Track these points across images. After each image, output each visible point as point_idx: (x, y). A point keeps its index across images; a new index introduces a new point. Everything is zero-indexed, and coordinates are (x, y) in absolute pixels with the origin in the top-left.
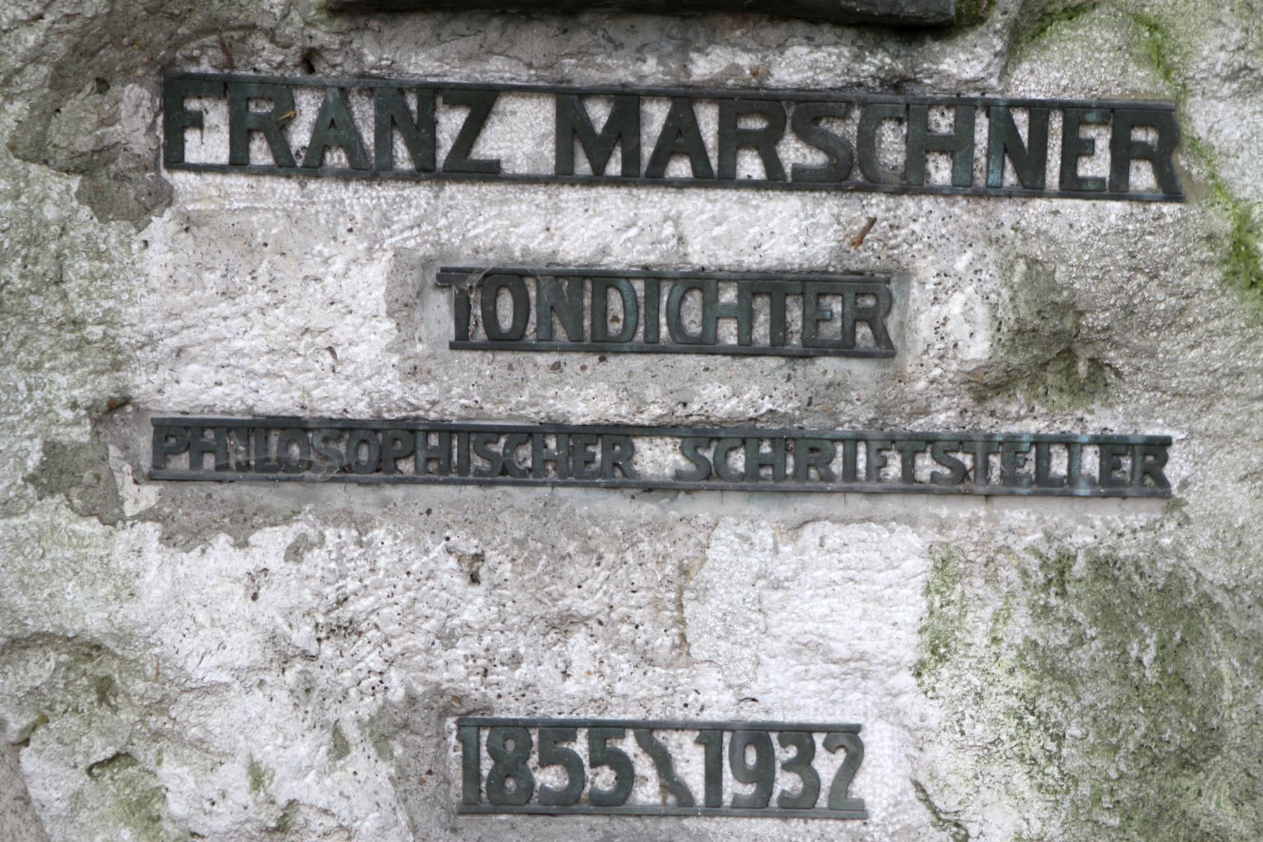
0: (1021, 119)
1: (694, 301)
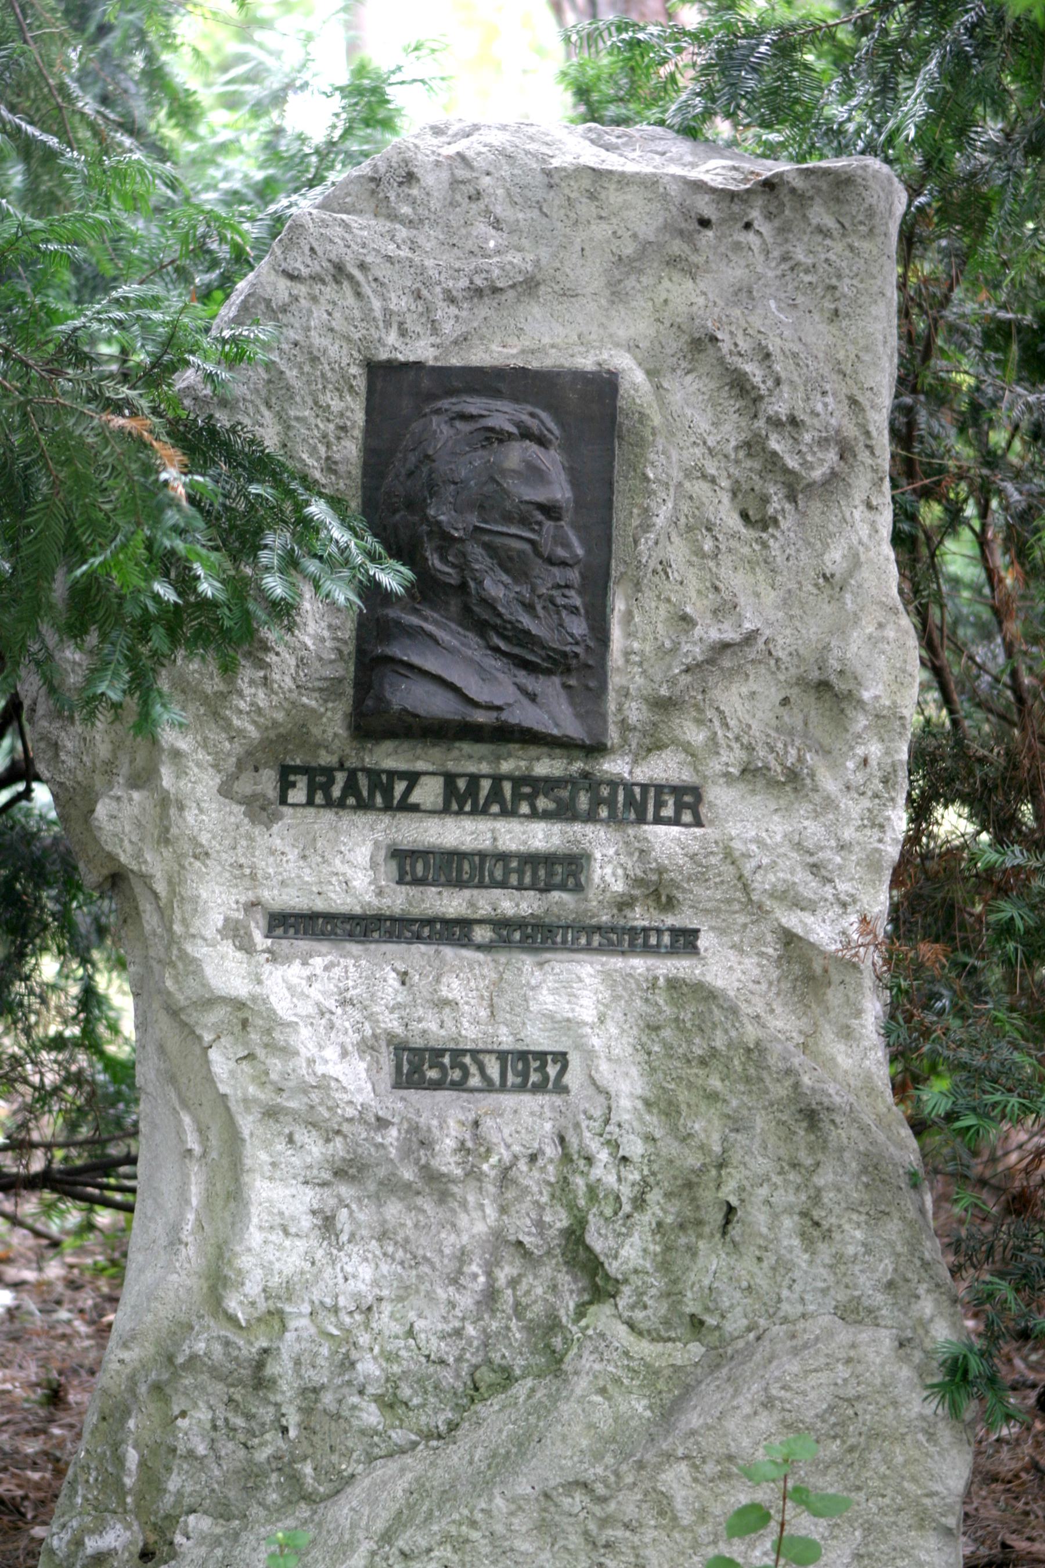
0: (637, 790)
1: (500, 865)
